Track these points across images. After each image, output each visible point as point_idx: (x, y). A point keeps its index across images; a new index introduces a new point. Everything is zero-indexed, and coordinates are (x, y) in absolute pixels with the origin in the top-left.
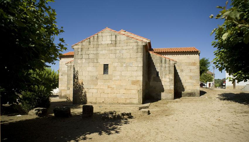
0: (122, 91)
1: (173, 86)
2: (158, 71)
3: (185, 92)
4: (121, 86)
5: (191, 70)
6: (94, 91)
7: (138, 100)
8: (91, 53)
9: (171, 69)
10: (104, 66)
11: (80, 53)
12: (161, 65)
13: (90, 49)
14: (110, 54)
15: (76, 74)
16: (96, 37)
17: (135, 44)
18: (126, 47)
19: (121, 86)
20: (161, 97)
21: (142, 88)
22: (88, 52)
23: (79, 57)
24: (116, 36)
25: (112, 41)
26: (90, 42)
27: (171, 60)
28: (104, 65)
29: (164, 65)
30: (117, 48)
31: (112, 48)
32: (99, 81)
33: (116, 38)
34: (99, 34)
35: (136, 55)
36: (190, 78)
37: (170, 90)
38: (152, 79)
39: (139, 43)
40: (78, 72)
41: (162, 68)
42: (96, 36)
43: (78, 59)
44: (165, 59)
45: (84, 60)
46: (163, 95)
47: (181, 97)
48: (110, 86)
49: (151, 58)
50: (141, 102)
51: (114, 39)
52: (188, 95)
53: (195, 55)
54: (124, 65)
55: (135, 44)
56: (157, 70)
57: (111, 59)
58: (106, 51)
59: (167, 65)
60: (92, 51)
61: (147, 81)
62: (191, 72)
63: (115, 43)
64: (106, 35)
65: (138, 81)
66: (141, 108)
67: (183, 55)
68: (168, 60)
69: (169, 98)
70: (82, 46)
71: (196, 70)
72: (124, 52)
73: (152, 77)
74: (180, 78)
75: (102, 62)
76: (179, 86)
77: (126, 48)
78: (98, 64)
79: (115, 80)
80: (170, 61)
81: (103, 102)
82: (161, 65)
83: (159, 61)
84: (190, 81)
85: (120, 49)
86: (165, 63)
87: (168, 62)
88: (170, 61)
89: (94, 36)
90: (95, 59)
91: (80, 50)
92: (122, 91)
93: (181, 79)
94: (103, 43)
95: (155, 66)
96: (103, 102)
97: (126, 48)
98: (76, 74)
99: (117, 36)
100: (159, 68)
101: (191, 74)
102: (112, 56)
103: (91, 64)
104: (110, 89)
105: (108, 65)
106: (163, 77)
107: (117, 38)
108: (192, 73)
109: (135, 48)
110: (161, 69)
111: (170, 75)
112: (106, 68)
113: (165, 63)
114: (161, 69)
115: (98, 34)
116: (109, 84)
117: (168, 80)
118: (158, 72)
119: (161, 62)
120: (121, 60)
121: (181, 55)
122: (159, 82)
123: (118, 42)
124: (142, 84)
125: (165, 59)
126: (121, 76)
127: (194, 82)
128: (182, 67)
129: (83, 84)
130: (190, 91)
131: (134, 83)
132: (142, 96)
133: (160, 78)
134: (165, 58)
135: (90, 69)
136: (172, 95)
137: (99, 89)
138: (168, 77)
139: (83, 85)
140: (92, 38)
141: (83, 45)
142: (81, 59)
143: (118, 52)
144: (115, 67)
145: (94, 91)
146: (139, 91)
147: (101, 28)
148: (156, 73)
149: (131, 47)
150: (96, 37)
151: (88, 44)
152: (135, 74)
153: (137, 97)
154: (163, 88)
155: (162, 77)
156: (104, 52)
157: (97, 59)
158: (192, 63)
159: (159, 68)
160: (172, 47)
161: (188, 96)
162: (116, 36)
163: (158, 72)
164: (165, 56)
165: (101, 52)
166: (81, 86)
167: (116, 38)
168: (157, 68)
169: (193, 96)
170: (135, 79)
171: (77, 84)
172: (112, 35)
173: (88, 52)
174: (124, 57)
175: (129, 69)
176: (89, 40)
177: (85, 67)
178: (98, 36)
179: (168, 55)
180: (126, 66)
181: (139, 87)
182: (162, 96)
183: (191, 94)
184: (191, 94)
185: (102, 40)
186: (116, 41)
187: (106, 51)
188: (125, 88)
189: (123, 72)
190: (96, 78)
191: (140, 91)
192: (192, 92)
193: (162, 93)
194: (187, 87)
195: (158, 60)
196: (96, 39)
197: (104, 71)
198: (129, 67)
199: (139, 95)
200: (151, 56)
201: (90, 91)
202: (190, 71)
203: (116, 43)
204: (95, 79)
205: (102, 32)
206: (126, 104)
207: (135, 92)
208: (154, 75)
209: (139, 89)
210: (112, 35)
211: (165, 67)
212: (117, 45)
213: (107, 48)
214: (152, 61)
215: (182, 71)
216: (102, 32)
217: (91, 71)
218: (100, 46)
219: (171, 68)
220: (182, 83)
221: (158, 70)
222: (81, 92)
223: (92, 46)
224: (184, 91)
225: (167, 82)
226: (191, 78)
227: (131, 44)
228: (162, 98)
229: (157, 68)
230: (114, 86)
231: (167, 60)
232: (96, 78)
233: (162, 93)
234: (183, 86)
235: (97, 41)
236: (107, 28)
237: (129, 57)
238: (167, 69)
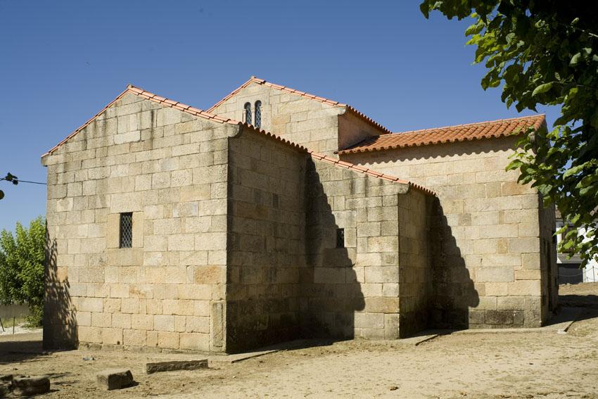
0: (170, 306)
1: (396, 286)
2: (340, 227)
3: (480, 306)
4: (166, 287)
5: (501, 213)
6: (96, 305)
7: (215, 337)
8: (90, 177)
9: (387, 217)
10: (122, 219)
11: (61, 181)
12: (352, 204)
13: (86, 164)
14: (138, 177)
15: (52, 252)
16: (100, 124)
17: (204, 136)
18: (179, 147)
19: (166, 288)
20: (353, 327)
21: (224, 296)
22: (81, 175)
23: (58, 193)
24: (152, 113)
25: (141, 130)
26: (86, 140)
27: (386, 182)
28: (122, 214)
29: (360, 202)
30: (158, 154)
31: (143, 156)
32: (107, 269)
33: (152, 120)
34: (108, 110)
35: (209, 175)
36: (500, 245)
37: (385, 299)
38: (320, 260)
39: (216, 131)
40: (56, 245)
41: (355, 214)
42: (101, 118)
43: (58, 199)
44: (367, 176)
45: (71, 200)
46: (360, 318)
47: (467, 328)
48: (136, 289)
49: (316, 177)
50: (224, 348)
51: (147, 124)
52: (491, 321)
53: (456, 156)
54: (175, 214)
55: (204, 136)
56: (337, 223)
57: (139, 193)
58: (127, 166)
59: (373, 202)
60: (90, 172)
61: (305, 266)
62: (501, 222)
63: (150, 138)
64: (127, 111)
65: (215, 267)
66: (178, 366)
67: (469, 153)
68: (377, 180)
69: (381, 333)
70: (65, 157)
71: (524, 213)
72: (174, 165)
73: (321, 250)
74: (458, 249)
75: (117, 206)
76: (456, 281)
77: (177, 151)
78: (105, 212)
79: (150, 266)
80: (381, 183)
81: (119, 343)
82: (352, 204)
83: (343, 186)
84: (499, 260)
85: (164, 156)
86: (366, 193)
87: (374, 189)
88: (381, 183)
89: (95, 121)
90: (98, 198)
91: (61, 169)
92: (170, 306)
93: (463, 253)
94: (120, 139)
95: (329, 207)
96: (119, 343)
97: (177, 151)
98: (52, 252)
99: (155, 111)
100: (344, 214)
101: (505, 232)
102: (142, 183)
103: (89, 215)
104: (136, 297)
105: (130, 214)
106: (360, 249)
107: (155, 119)
108: (508, 227)
109: (206, 148)
110: (351, 218)
111: (384, 240)
112: (126, 220)
113: (366, 193)
114: (351, 218)
115: (105, 112)
116: (133, 281)
117: (376, 260)
118: (343, 229)
119: (352, 188)
120: (164, 194)
121: (460, 155)
122: (343, 270)
123: (158, 133)
124: (225, 280)
125: (367, 176)
126: (166, 251)
127: (516, 262)
128: (464, 205)
129: (68, 284)
130: (500, 304)
131: (202, 275)
132: (225, 325)
133: (351, 255)
134: (364, 175)
135: (85, 230)
136: (391, 322)
137: (108, 299)
138: (375, 248)
139: (69, 287)
140: (91, 126)
141: (70, 150)
142: (64, 198)
143: (157, 166)
144: (150, 222)
145: (96, 305)
146: (215, 305)
147: (114, 96)
148: (334, 236)
149: (194, 148)
150: (100, 124)
151: (80, 148)
152: (205, 242)
153: (212, 325)
154: (362, 295)
155: (355, 249)
156: (121, 171)
157: (103, 198)
158: (507, 183)
159: (344, 214)
160: (451, 125)
161: (494, 326)
162: (152, 113)
163: (343, 229)
164: (367, 166)
165: (114, 174)
166: (64, 290)
167: (152, 120)
168: (338, 217)
169: (513, 325)
170: (204, 263)
171: (54, 285)
172: (141, 111)
173: (81, 175)
174: (175, 184)
175: (189, 225)
176: (85, 134)
177: (73, 224)
178: (105, 119)
179: (410, 159)
180: (180, 218)
181: (216, 290)
182: (355, 322)
183: (505, 318)
184: (505, 318)
185: (115, 132)
186: (152, 131)
187: (127, 166)
188: (176, 297)
189: (170, 238)
190: (101, 261)
191: (219, 306)
192: (511, 305)
193: (356, 311)
194: (487, 285)
195: (341, 184)
196: (100, 129)
197: (121, 236)
198: (187, 219)
199: (215, 320)
200: (317, 170)
201: (85, 304)
202: (497, 220)
203: (152, 139)
204: (97, 263)
205: (116, 105)
206: (179, 352)
207: (203, 308)
208: (326, 244)
209: (216, 299)
210: (141, 111)
211: (367, 210)
212: (156, 144)
213: (129, 158)
214: (320, 187)
215: (466, 219)
216: (116, 105)
217: (87, 238)
218: (111, 153)
219: (386, 210)
220: (467, 272)
221: (340, 223)
222: (65, 311)
223: (90, 153)
224: (476, 302)
225: (376, 266)
226: (504, 246)
227: (194, 137)
228: (356, 333)
229: (338, 217)
230: (148, 288)
231: (374, 180)
232: (101, 261)
233: (356, 311)
234: (472, 283)
235: (105, 136)
236: (253, 77)
237: (187, 183)
238: (373, 216)
